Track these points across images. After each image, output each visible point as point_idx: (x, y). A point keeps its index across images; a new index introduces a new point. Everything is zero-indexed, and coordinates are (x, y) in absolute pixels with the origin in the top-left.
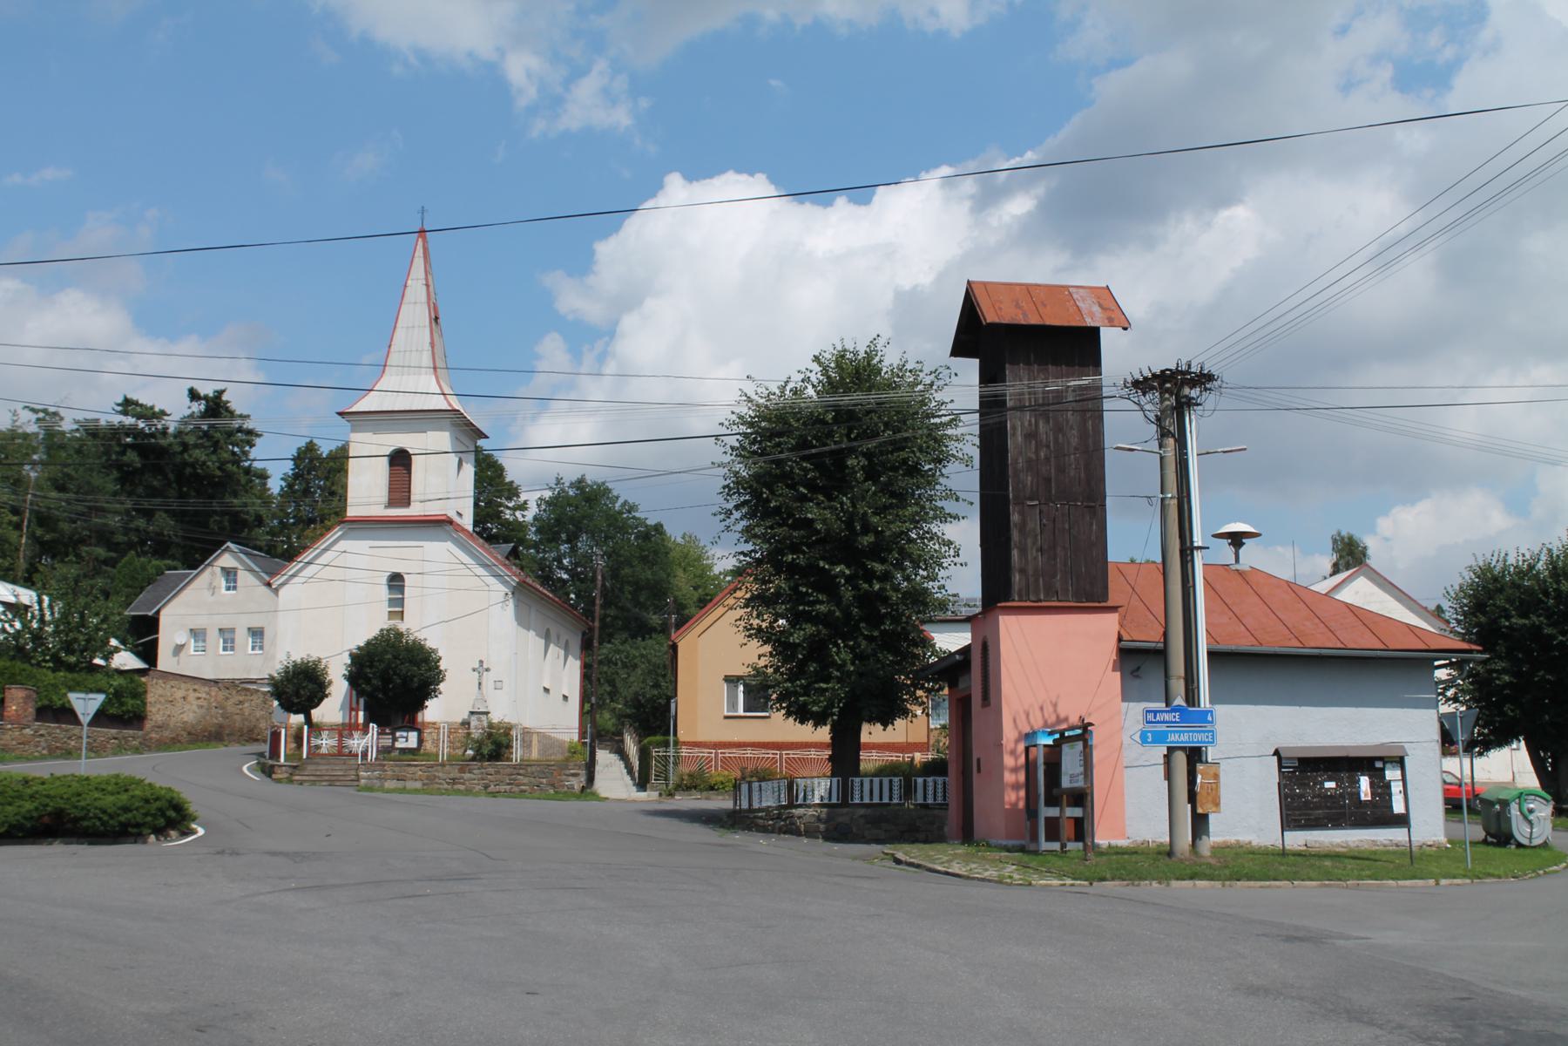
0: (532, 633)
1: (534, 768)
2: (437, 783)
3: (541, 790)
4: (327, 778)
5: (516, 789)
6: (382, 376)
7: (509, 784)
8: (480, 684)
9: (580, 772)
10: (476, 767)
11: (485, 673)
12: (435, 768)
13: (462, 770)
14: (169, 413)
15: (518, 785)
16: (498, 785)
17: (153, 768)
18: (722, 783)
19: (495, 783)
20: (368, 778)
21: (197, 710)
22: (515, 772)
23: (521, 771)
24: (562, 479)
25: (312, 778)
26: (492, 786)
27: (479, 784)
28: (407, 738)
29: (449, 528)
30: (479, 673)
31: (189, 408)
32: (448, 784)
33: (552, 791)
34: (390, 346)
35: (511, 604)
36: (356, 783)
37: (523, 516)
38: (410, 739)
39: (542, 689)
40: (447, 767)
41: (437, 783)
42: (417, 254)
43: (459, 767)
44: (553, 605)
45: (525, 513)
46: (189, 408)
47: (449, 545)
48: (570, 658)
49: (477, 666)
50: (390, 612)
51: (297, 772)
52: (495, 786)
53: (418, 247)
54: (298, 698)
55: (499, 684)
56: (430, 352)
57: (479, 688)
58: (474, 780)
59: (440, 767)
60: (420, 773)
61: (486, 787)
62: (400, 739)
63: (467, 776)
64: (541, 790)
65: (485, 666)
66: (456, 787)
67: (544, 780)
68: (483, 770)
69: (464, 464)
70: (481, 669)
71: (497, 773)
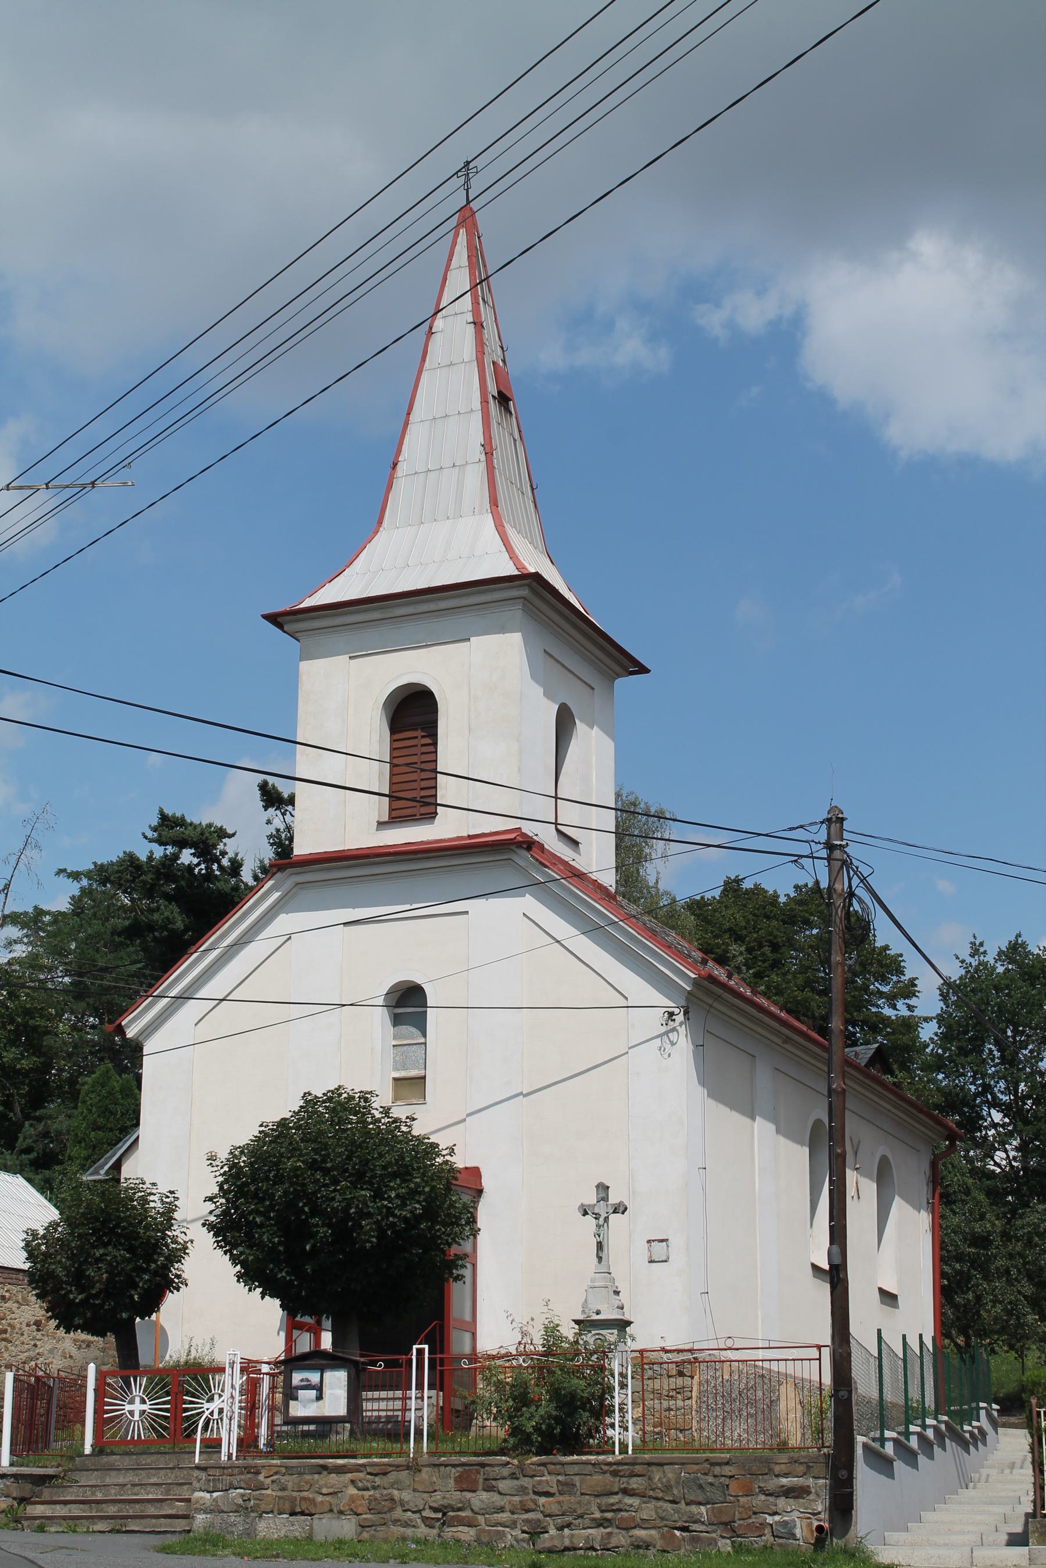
0: (762, 1128)
1: (670, 1472)
2: (396, 1522)
3: (695, 1540)
4: (112, 1510)
5: (620, 1539)
6: (376, 532)
7: (599, 1524)
8: (600, 1246)
9: (810, 1482)
10: (506, 1471)
11: (613, 1218)
12: (392, 1477)
13: (466, 1484)
14: (230, 831)
15: (626, 1527)
16: (568, 1525)
17: (809, 1467)
19: (559, 1521)
20: (214, 1510)
21: (74, 1351)
22: (617, 1484)
23: (635, 1483)
24: (981, 944)
25: (76, 1511)
26: (553, 1531)
27: (513, 1525)
28: (319, 1389)
29: (523, 858)
30: (597, 1216)
31: (269, 822)
32: (428, 1522)
33: (725, 1545)
34: (395, 465)
35: (683, 1043)
36: (181, 1525)
37: (910, 1008)
38: (327, 1391)
39: (809, 1270)
40: (425, 1474)
41: (396, 1522)
42: (454, 263)
43: (454, 1472)
44: (807, 1051)
45: (913, 1002)
46: (269, 822)
47: (529, 903)
48: (898, 1207)
50: (395, 1079)
51: (47, 1493)
52: (561, 1529)
53: (457, 248)
54: (81, 1289)
55: (659, 1250)
56: (483, 465)
57: (600, 1259)
58: (502, 1510)
59: (404, 1474)
60: (352, 1491)
61: (535, 1532)
62: (301, 1393)
63: (481, 1498)
64: (695, 1540)
65: (613, 1199)
66: (449, 1532)
67: (703, 1509)
68: (526, 1482)
69: (580, 727)
70: (602, 1209)
71: (566, 1488)
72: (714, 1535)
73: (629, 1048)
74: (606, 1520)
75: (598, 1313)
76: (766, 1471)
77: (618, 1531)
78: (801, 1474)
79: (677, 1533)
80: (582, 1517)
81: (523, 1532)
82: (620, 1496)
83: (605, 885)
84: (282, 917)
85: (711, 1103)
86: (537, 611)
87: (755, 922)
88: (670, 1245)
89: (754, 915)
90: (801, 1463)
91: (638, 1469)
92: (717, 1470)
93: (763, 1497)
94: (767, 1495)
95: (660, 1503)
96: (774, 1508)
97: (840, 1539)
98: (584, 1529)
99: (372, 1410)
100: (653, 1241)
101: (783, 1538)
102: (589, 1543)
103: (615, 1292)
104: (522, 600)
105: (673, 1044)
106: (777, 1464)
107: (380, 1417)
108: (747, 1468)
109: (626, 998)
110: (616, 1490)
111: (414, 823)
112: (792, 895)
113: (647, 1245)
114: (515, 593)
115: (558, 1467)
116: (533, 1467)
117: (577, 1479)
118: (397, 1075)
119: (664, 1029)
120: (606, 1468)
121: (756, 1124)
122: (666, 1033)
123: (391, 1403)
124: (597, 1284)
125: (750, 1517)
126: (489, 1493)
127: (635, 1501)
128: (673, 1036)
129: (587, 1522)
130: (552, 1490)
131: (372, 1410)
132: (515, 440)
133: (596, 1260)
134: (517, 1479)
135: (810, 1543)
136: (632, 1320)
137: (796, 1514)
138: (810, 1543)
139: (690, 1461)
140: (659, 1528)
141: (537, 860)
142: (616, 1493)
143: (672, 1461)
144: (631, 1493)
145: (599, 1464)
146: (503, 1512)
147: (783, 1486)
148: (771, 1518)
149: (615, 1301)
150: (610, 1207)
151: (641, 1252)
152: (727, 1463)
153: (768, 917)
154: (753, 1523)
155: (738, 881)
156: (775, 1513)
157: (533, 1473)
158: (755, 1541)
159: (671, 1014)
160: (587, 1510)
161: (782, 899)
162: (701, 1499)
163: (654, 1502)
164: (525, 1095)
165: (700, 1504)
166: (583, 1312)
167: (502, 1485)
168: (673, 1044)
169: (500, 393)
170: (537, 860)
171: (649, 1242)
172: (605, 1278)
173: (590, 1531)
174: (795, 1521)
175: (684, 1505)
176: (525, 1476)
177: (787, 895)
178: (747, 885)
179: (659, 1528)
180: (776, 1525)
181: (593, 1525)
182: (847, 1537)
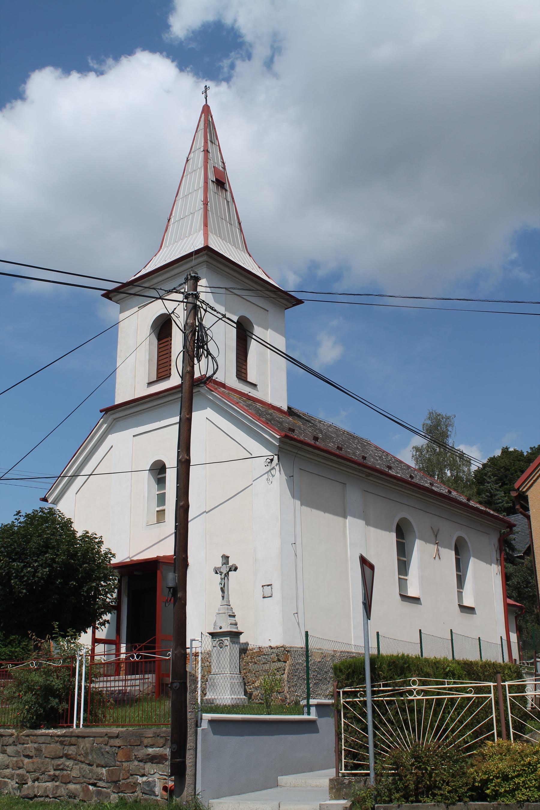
7: (54, 778)
18: (506, 778)
23: (72, 750)
27: (11, 778)
49: (219, 564)
50: (157, 511)
52: (34, 781)
55: (268, 589)
58: (7, 767)
61: (22, 783)
67: (104, 770)
68: (19, 747)
70: (224, 570)
72: (109, 790)
73: (253, 481)
74: (57, 776)
75: (221, 628)
76: (139, 743)
77: (61, 784)
78: (161, 745)
79: (91, 787)
80: (44, 773)
81: (17, 783)
82: (64, 759)
83: (278, 407)
84: (110, 437)
85: (305, 509)
86: (219, 270)
87: (514, 463)
88: (273, 587)
89: (514, 460)
90: (162, 737)
91: (73, 740)
92: (113, 742)
93: (136, 763)
94: (140, 761)
95: (83, 765)
96: (142, 771)
97: (178, 797)
98: (45, 782)
99: (119, 686)
100: (265, 586)
101: (147, 794)
102: (46, 792)
103: (230, 616)
104: (205, 263)
105: (273, 476)
106: (146, 737)
107: (115, 691)
108: (128, 741)
109: (251, 455)
110: (61, 755)
111: (162, 381)
112: (530, 451)
113: (262, 588)
114: (201, 259)
115: (35, 737)
116: (23, 737)
117: (44, 746)
118: (158, 509)
119: (268, 468)
120: (57, 739)
121: (347, 521)
122: (270, 471)
123: (105, 683)
124: (220, 612)
125: (128, 778)
126: (27, 754)
127: (70, 763)
128: (273, 472)
129: (46, 777)
130: (31, 754)
131: (119, 686)
132: (228, 202)
133: (221, 598)
134: (16, 745)
135: (165, 799)
136: (243, 631)
137: (157, 776)
138: (165, 799)
139: (98, 735)
140: (82, 783)
141: (209, 388)
142: (62, 757)
143: (89, 735)
144: (69, 757)
145: (54, 736)
146: (8, 768)
147: (149, 755)
148: (141, 778)
149: (232, 620)
150: (228, 567)
151: (259, 592)
152: (117, 737)
153: (519, 461)
154: (130, 782)
155: (507, 448)
156: (143, 775)
157: (23, 742)
158: (130, 796)
159: (272, 460)
160: (47, 768)
161: (525, 454)
162: (103, 763)
163: (80, 764)
164: (207, 513)
165: (103, 766)
166: (214, 628)
167: (10, 750)
168: (273, 476)
169: (216, 179)
170: (209, 388)
171: (263, 586)
172: (225, 608)
173: (48, 784)
174: (155, 782)
175: (95, 767)
176: (20, 744)
177: (527, 452)
178: (511, 449)
179: (82, 783)
180: (143, 784)
181: (49, 780)
182: (182, 796)
